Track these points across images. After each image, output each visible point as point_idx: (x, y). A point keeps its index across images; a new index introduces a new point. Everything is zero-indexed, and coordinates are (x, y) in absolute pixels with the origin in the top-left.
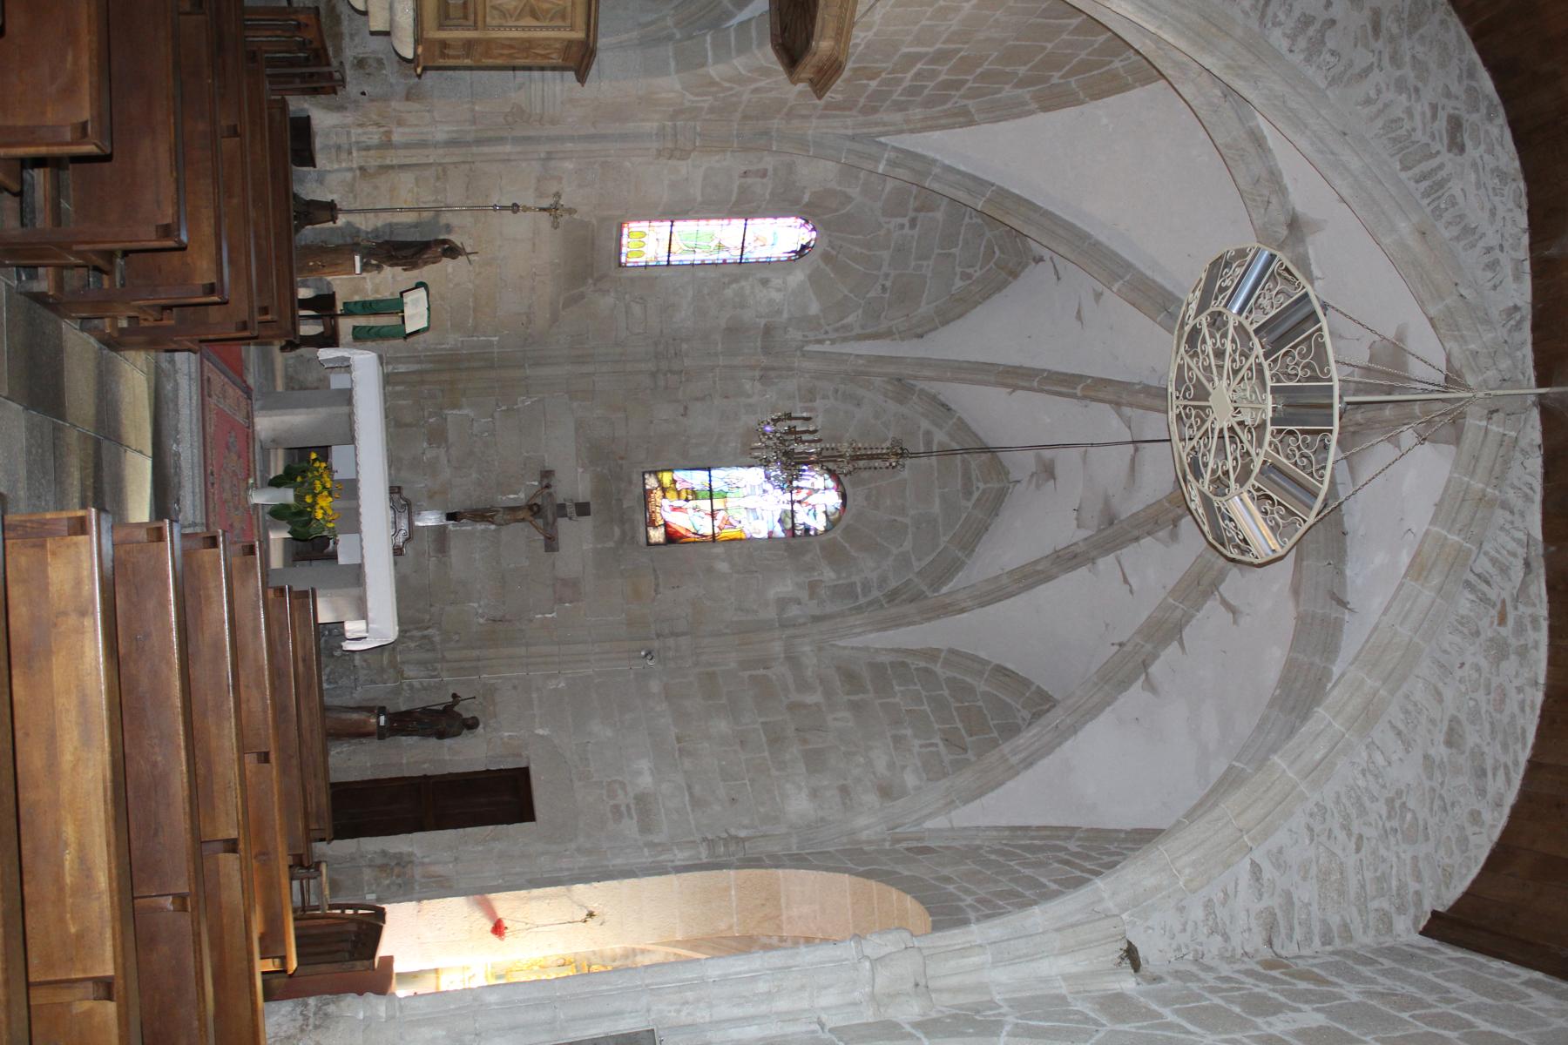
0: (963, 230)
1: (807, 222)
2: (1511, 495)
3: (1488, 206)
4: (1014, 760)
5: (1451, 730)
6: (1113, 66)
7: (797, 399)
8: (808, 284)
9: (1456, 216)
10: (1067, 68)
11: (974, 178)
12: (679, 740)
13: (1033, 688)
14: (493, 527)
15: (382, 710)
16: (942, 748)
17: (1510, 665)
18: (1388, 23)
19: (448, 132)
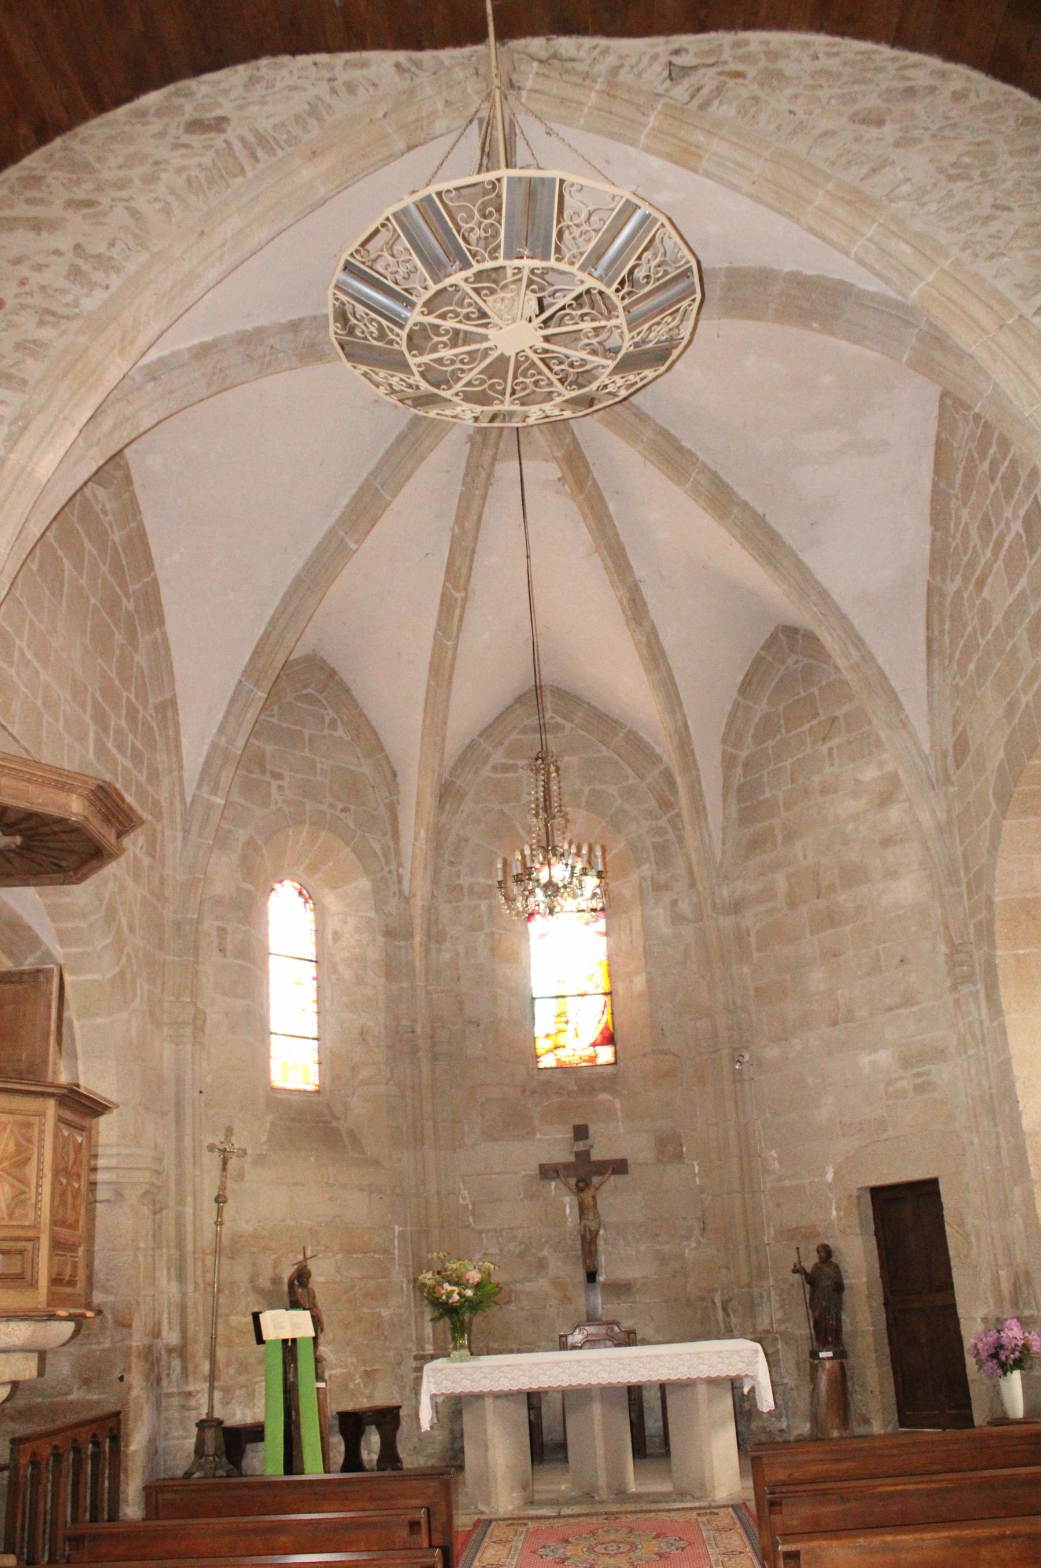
0: (285, 725)
1: (273, 889)
2: (602, 68)
3: (286, 93)
4: (856, 656)
5: (864, 121)
6: (117, 540)
7: (460, 904)
8: (340, 890)
9: (297, 123)
10: (118, 590)
11: (233, 700)
12: (835, 1023)
13: (763, 654)
14: (602, 1232)
15: (814, 1355)
16: (832, 743)
17: (788, 67)
18: (80, 193)
19: (169, 1280)
